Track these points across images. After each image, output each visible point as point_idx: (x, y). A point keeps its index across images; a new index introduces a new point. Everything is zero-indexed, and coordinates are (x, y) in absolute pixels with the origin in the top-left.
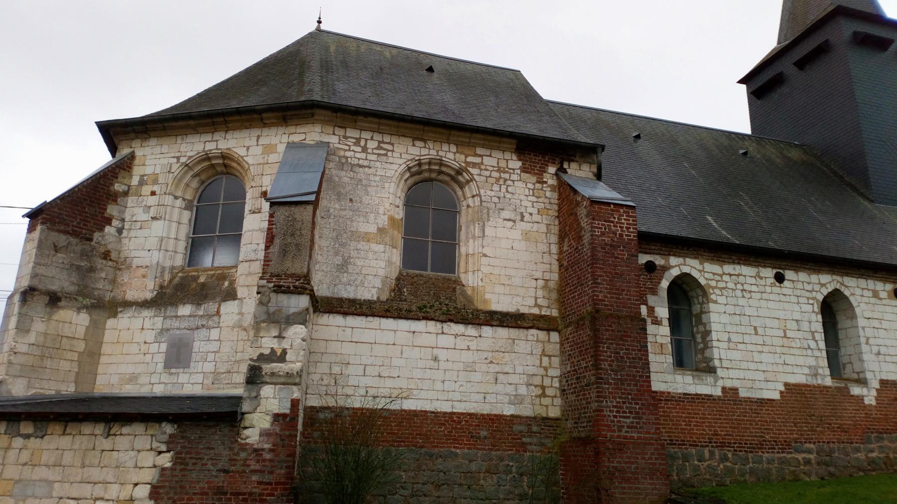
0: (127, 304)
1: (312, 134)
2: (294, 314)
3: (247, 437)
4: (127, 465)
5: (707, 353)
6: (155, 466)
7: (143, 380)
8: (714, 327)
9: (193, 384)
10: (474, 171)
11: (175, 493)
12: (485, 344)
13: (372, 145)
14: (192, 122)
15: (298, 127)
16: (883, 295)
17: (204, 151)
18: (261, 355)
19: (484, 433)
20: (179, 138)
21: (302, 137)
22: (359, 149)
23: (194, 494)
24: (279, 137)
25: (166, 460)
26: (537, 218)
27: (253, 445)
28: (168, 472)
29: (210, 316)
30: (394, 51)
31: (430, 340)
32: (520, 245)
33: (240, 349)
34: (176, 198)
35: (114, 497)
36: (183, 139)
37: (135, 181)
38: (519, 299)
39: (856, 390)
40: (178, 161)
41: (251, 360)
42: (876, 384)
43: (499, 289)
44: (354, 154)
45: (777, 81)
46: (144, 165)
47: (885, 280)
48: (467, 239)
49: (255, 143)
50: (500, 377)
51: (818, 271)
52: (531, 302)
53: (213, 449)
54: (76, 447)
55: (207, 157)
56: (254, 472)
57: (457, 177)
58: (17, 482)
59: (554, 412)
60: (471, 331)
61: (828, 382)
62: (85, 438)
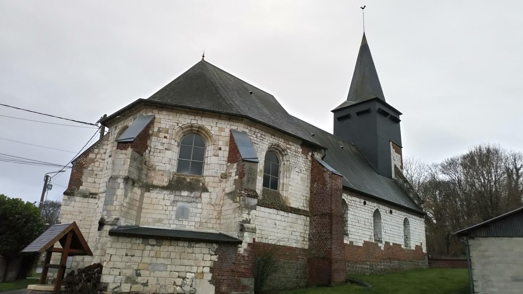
0: (155, 187)
1: (240, 127)
5: (345, 228)
8: (349, 219)
10: (288, 151)
12: (289, 220)
13: (259, 135)
14: (187, 110)
16: (388, 212)
18: (243, 220)
19: (288, 253)
22: (255, 136)
25: (215, 258)
26: (305, 172)
29: (197, 198)
31: (273, 216)
32: (300, 182)
34: (176, 141)
35: (195, 271)
37: (156, 129)
38: (298, 203)
39: (380, 245)
40: (178, 125)
42: (384, 243)
43: (293, 199)
44: (253, 138)
45: (347, 117)
47: (389, 207)
48: (284, 177)
50: (293, 232)
51: (374, 202)
52: (302, 205)
54: (177, 251)
55: (192, 126)
56: (243, 264)
57: (282, 152)
58: (149, 264)
59: (307, 247)
60: (286, 214)
61: (374, 241)
62: (180, 247)
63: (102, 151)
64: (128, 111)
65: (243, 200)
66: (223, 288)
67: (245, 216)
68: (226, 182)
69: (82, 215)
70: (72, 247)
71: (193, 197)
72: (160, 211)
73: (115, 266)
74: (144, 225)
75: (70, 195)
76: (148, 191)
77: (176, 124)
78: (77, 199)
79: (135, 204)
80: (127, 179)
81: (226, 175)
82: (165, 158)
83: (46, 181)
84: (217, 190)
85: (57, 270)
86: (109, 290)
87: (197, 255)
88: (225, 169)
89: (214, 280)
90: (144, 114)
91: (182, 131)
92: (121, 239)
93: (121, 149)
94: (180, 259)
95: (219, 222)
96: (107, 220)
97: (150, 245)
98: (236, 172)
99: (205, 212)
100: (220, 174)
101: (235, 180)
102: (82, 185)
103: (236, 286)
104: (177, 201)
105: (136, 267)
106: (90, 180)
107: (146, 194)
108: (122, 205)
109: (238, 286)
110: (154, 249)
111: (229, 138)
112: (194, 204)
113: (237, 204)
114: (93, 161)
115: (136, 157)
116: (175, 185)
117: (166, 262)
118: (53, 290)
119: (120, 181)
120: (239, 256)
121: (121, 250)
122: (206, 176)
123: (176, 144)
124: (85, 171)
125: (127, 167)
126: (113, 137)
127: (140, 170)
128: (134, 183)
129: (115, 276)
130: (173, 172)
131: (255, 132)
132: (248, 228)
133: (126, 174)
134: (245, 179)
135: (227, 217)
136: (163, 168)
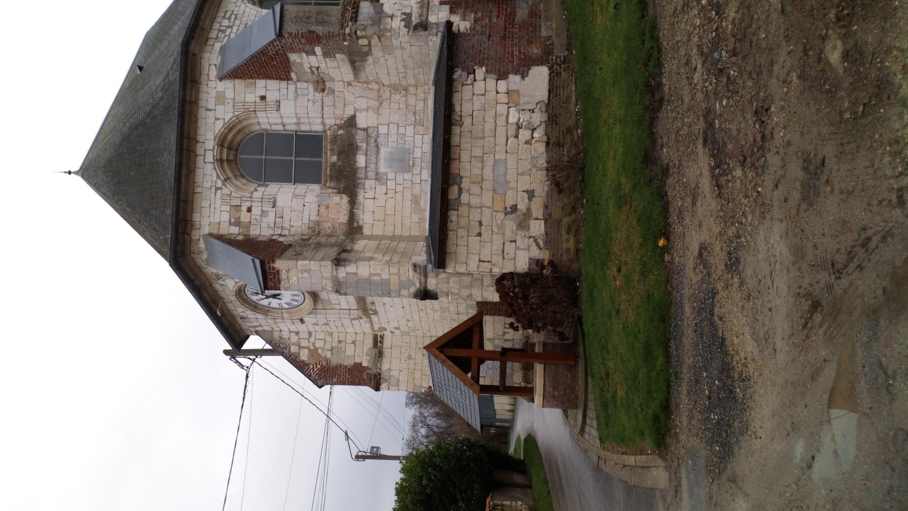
0: (352, 217)
1: (211, 61)
6: (485, 80)
13: (226, 23)
14: (184, 171)
17: (213, 163)
18: (405, 26)
21: (213, 68)
22: (229, 30)
29: (368, 136)
30: (109, 119)
33: (396, 106)
34: (256, 190)
35: (506, 107)
40: (221, 189)
41: (408, 32)
44: (233, 33)
54: (469, 146)
56: (490, 20)
58: (494, 190)
62: (462, 141)
63: (294, 339)
64: (205, 294)
65: (364, 30)
66: (536, 51)
67: (397, 23)
69: (413, 325)
70: (469, 346)
71: (367, 144)
72: (395, 201)
73: (500, 252)
74: (424, 229)
77: (219, 192)
78: (385, 366)
80: (338, 262)
81: (318, 82)
82: (292, 206)
83: (364, 457)
84: (349, 98)
85: (509, 364)
86: (541, 257)
87: (476, 108)
88: (305, 85)
89: (522, 69)
90: (205, 256)
91: (233, 180)
92: (451, 248)
93: (279, 282)
95: (412, 89)
96: (418, 285)
97: (459, 196)
98: (308, 54)
99: (395, 118)
100: (317, 94)
101: (326, 54)
102: (361, 364)
103: (531, 29)
104: (377, 174)
105: (501, 216)
106: (350, 351)
107: (367, 231)
110: (467, 187)
111: (237, 81)
112: (381, 140)
113: (373, 42)
114: (314, 352)
116: (347, 181)
117: (489, 162)
119: (342, 272)
120: (475, 28)
121: (471, 245)
122: (324, 124)
123: (261, 189)
124: (334, 362)
125: (313, 265)
126: (263, 322)
127: (319, 246)
130: (321, 188)
131: (219, 31)
132: (421, 15)
134: (320, 30)
136: (314, 207)
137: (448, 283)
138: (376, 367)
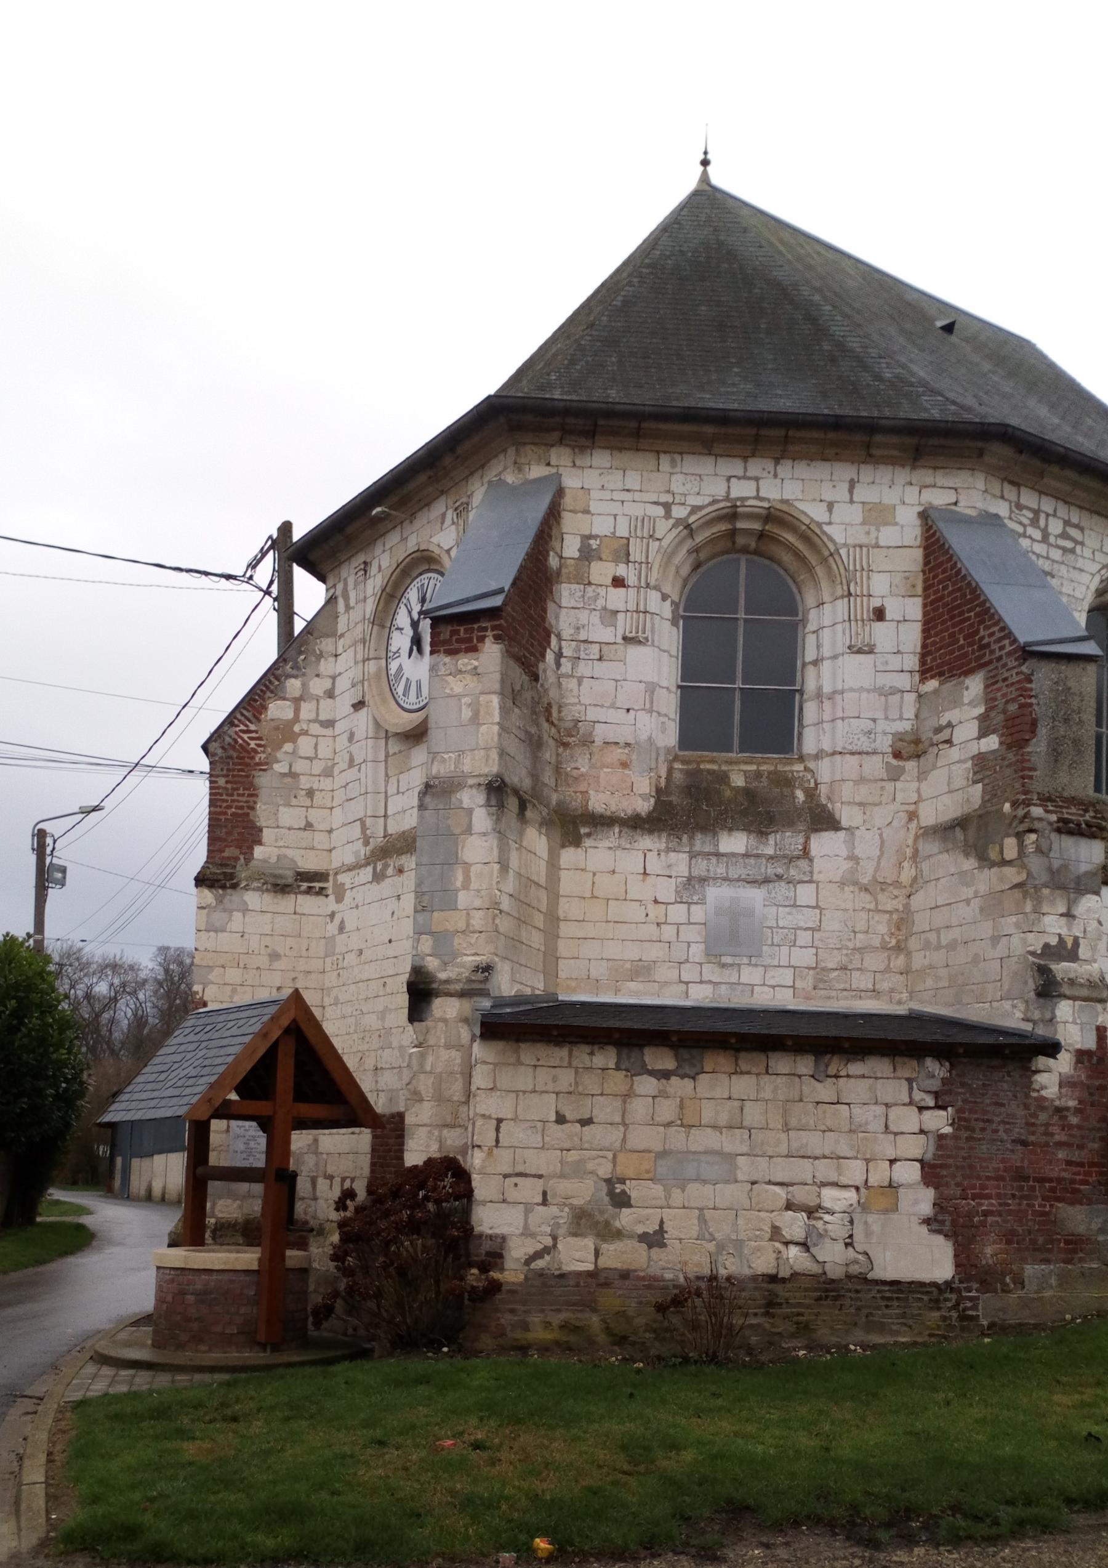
0: (602, 822)
2: (1086, 873)
3: (1043, 1088)
4: (870, 1128)
6: (922, 1132)
7: (666, 973)
9: (773, 987)
11: (965, 1177)
14: (709, 429)
15: (940, 473)
17: (727, 498)
18: (1046, 946)
20: (665, 460)
22: (1037, 534)
23: (988, 1178)
24: (897, 490)
27: (1053, 1100)
28: (950, 1142)
29: (791, 859)
33: (861, 926)
34: (664, 597)
35: (859, 1180)
36: (673, 463)
40: (668, 515)
44: (1031, 544)
46: (587, 512)
49: (847, 497)
53: (1003, 1105)
54: (767, 1094)
56: (1060, 1144)
62: (779, 1080)
63: (318, 686)
65: (1039, 850)
66: (989, 1250)
67: (1053, 927)
68: (922, 776)
69: (347, 963)
70: (300, 1096)
72: (640, 923)
73: (520, 1168)
74: (574, 990)
75: (224, 887)
76: (576, 841)
77: (660, 511)
79: (535, 903)
80: (497, 790)
81: (917, 741)
82: (626, 683)
84: (880, 816)
85: (258, 1188)
86: (509, 1264)
87: (857, 1110)
88: (910, 713)
90: (510, 478)
91: (689, 544)
92: (529, 1053)
94: (787, 1128)
95: (899, 962)
96: (442, 976)
97: (652, 1073)
98: (983, 719)
99: (833, 923)
101: (981, 762)
103: (1041, 1240)
104: (703, 880)
105: (605, 1170)
106: (289, 816)
107: (569, 856)
108: (495, 906)
109: (1052, 1242)
110: (671, 1090)
111: (919, 554)
112: (781, 890)
114: (287, 732)
115: (518, 687)
116: (686, 810)
117: (731, 1143)
118: (255, 1267)
119: (472, 799)
120: (1043, 1108)
121: (535, 1099)
122: (819, 756)
123: (667, 609)
124: (264, 781)
125: (489, 732)
126: (356, 615)
127: (535, 744)
128: (523, 806)
129: (528, 1208)
130: (668, 750)
131: (1037, 512)
132: (1072, 982)
133: (493, 767)
134: (1039, 747)
135: (946, 938)
136: (623, 734)
137: (448, 1047)
138: (251, 879)
